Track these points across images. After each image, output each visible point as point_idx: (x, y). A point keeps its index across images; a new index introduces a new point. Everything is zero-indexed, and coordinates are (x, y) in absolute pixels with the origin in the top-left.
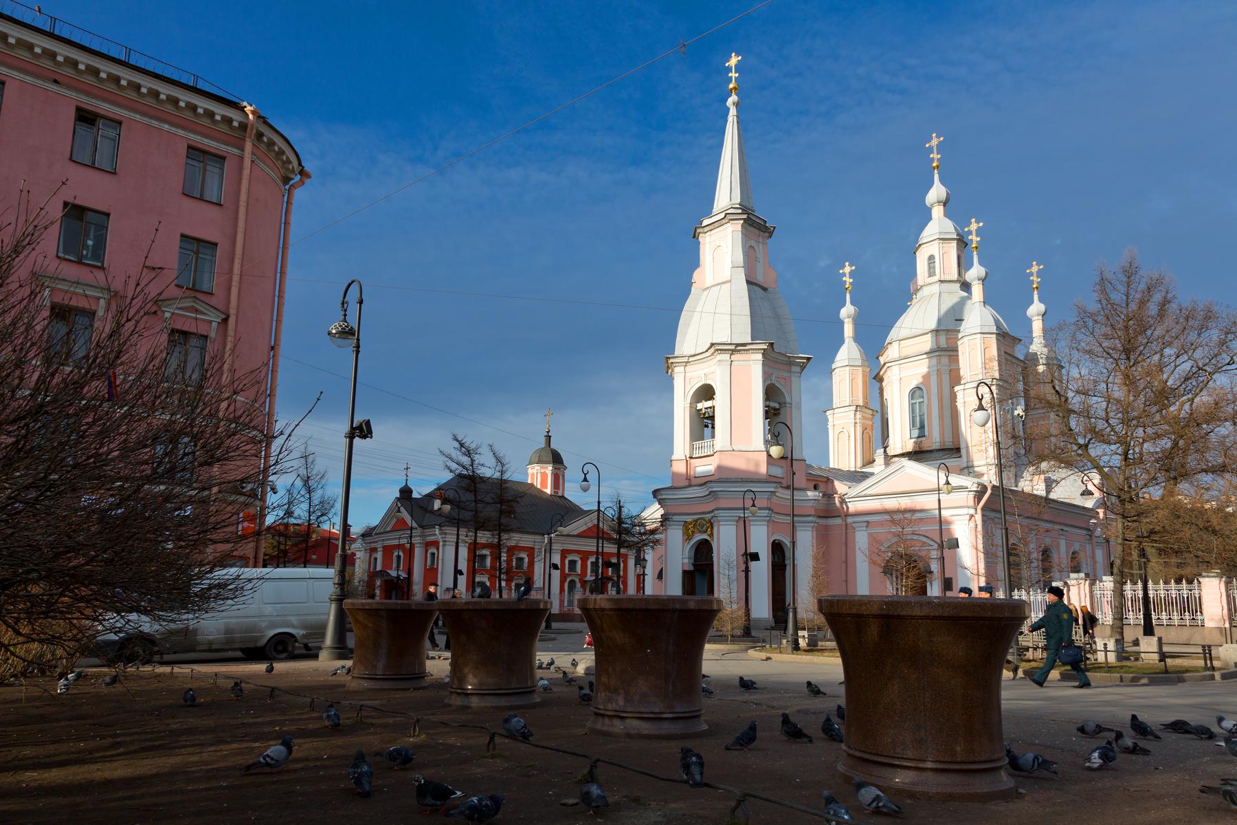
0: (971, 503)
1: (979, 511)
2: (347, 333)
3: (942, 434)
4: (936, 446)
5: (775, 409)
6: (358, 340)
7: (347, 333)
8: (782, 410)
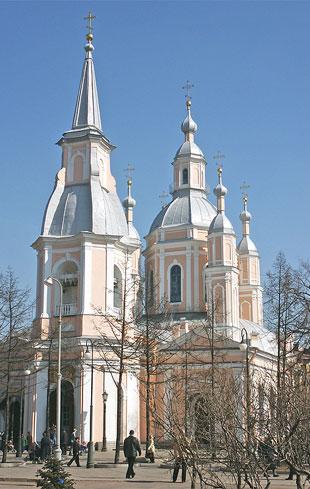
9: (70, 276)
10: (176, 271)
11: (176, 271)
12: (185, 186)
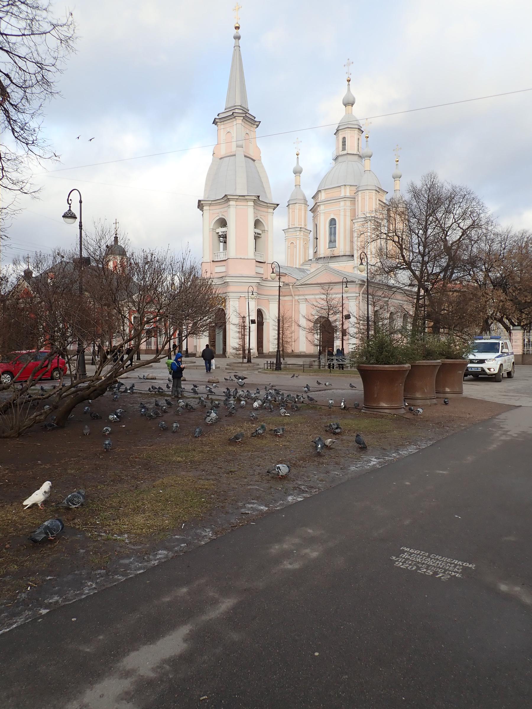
0: (357, 291)
1: (361, 294)
2: (69, 215)
3: (471, 367)
4: (342, 254)
5: (258, 234)
6: (81, 222)
7: (69, 215)
8: (262, 235)
9: (224, 229)
10: (333, 222)
11: (333, 222)
12: (345, 152)
